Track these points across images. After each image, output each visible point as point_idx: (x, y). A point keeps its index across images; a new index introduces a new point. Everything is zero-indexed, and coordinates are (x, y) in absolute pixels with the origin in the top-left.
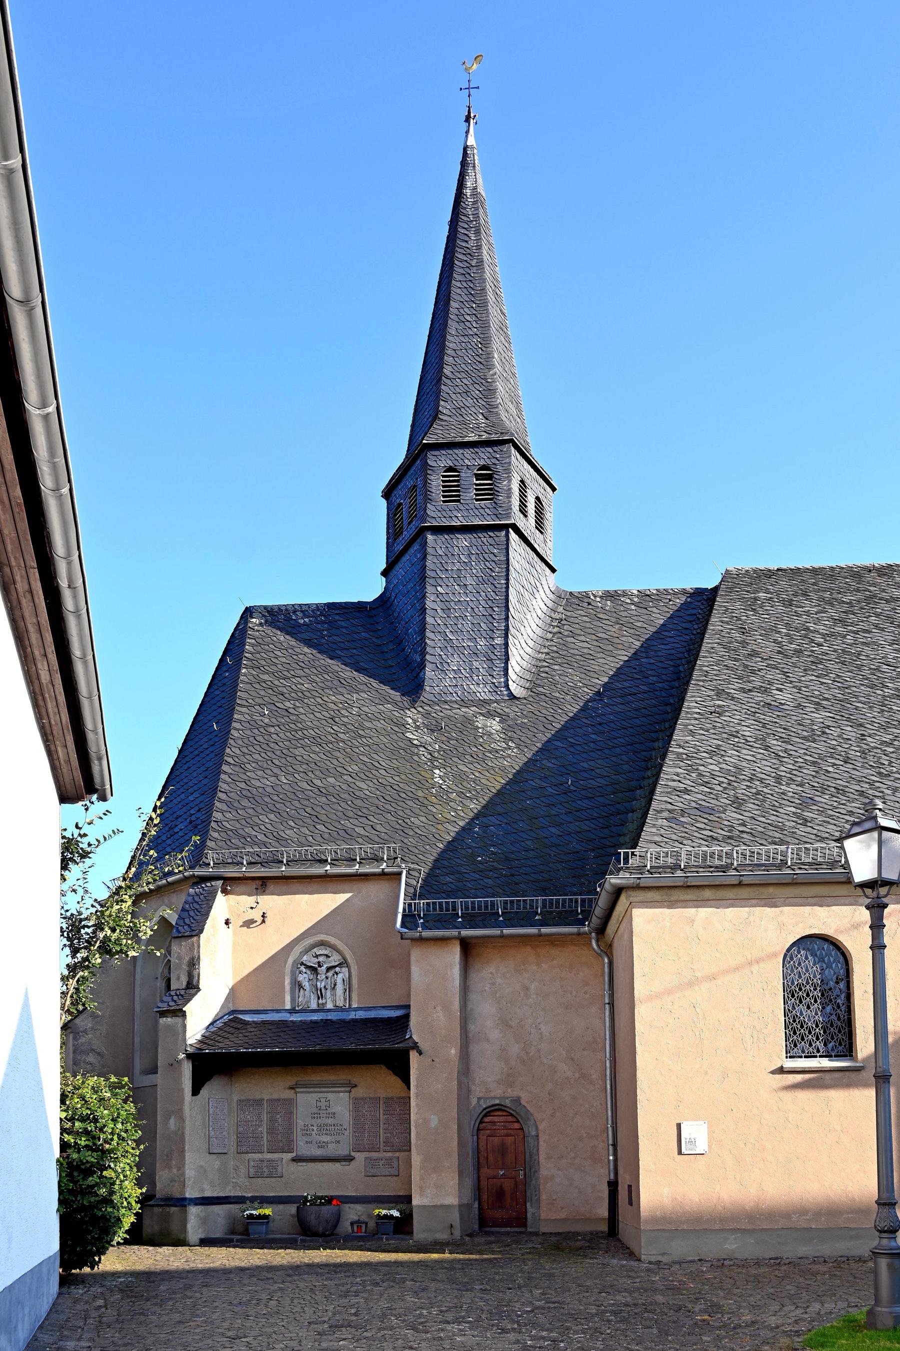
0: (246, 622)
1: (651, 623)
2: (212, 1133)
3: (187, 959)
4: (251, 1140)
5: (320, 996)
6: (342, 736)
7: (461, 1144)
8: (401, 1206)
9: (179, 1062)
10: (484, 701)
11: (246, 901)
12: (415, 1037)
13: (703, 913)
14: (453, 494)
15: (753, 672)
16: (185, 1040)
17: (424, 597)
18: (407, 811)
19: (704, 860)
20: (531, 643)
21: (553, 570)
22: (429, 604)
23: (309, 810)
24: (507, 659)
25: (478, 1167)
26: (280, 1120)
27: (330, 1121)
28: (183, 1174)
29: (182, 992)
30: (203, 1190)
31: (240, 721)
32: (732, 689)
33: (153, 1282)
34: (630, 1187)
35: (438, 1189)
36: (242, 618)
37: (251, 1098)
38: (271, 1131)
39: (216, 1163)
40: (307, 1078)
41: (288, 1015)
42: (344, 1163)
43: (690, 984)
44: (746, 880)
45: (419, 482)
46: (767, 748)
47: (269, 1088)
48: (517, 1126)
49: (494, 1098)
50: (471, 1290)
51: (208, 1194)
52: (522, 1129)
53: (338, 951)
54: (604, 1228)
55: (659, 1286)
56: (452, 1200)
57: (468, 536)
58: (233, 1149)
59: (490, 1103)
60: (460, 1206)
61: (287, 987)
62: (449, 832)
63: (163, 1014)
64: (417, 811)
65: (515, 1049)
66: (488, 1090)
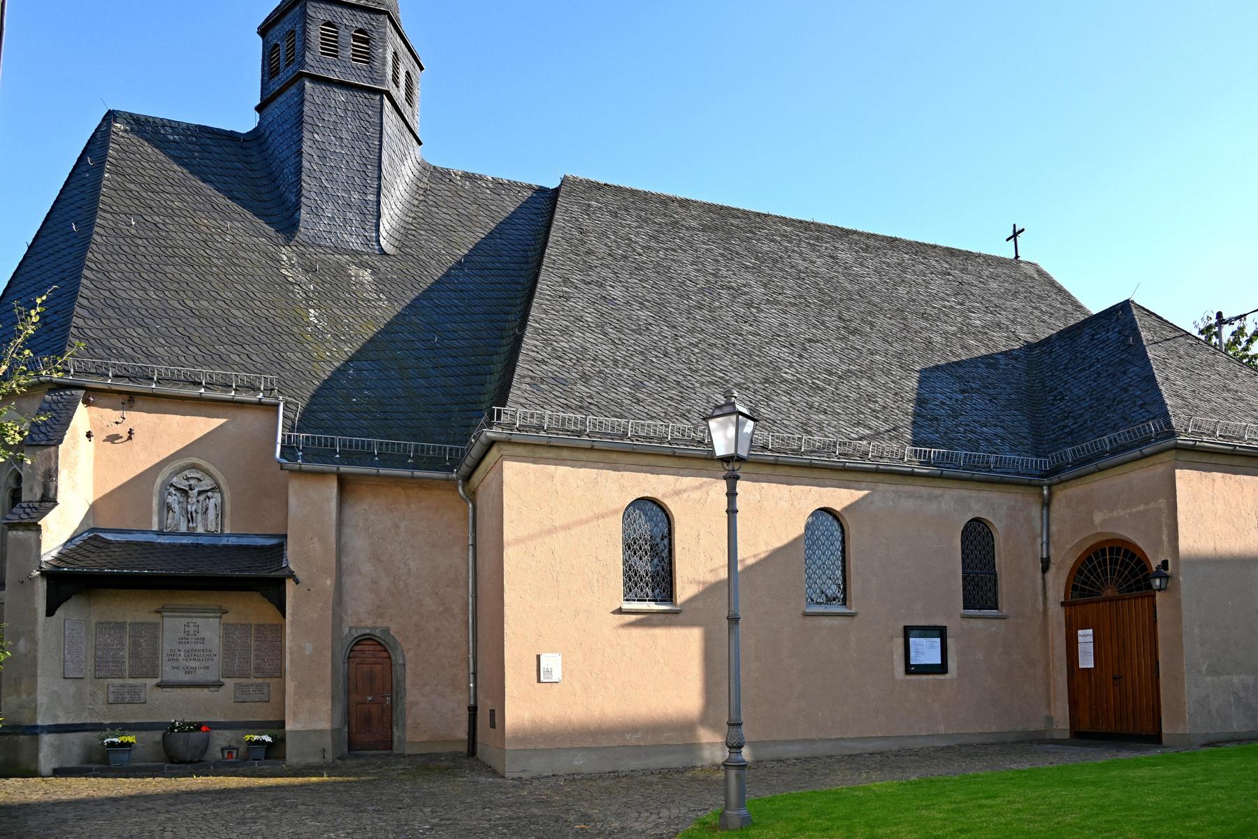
0: (109, 126)
1: (504, 208)
2: (68, 657)
3: (42, 469)
5: (191, 519)
6: (215, 261)
7: (334, 671)
8: (275, 732)
9: (32, 580)
10: (357, 252)
11: (111, 415)
12: (291, 566)
13: (562, 470)
14: (331, 47)
15: (591, 267)
16: (39, 556)
17: (301, 140)
18: (284, 346)
19: (563, 424)
20: (400, 206)
21: (420, 143)
22: (305, 148)
23: (180, 329)
24: (379, 217)
25: (348, 693)
27: (199, 646)
28: (35, 700)
29: (36, 505)
31: (103, 227)
32: (576, 278)
33: (17, 817)
34: (492, 712)
35: (311, 715)
36: (104, 119)
38: (134, 655)
39: (72, 688)
43: (550, 532)
44: (597, 445)
45: (298, 28)
46: (605, 334)
47: (133, 611)
48: (385, 654)
49: (366, 628)
50: (365, 811)
51: (62, 721)
52: (389, 657)
53: (211, 476)
54: (463, 748)
55: (530, 799)
56: (325, 725)
57: (345, 92)
58: (90, 674)
59: (360, 633)
60: (333, 731)
62: (326, 372)
63: (12, 526)
64: (293, 347)
65: (385, 582)
66: (360, 621)
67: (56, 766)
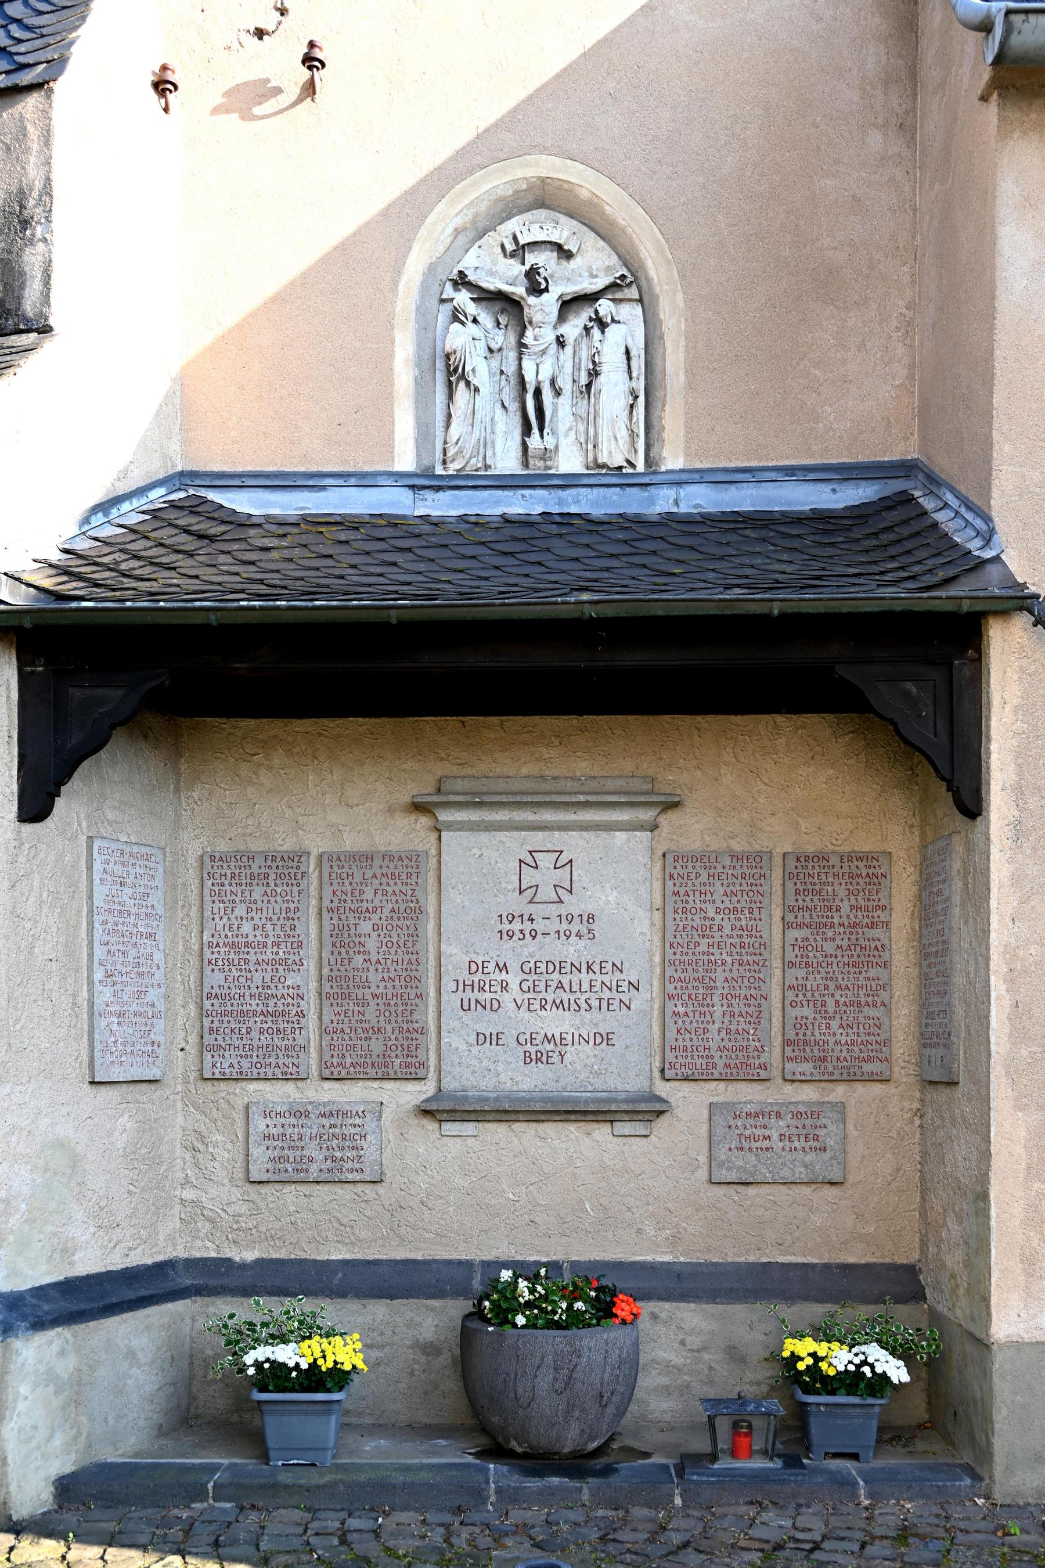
2: (104, 995)
4: (256, 1023)
5: (533, 420)
26: (372, 944)
27: (573, 950)
30: (67, 1251)
37: (256, 845)
38: (339, 987)
40: (482, 767)
41: (407, 495)
42: (626, 1128)
47: (326, 803)
51: (88, 1263)
58: (181, 1064)
61: (404, 376)
67: (65, 1465)
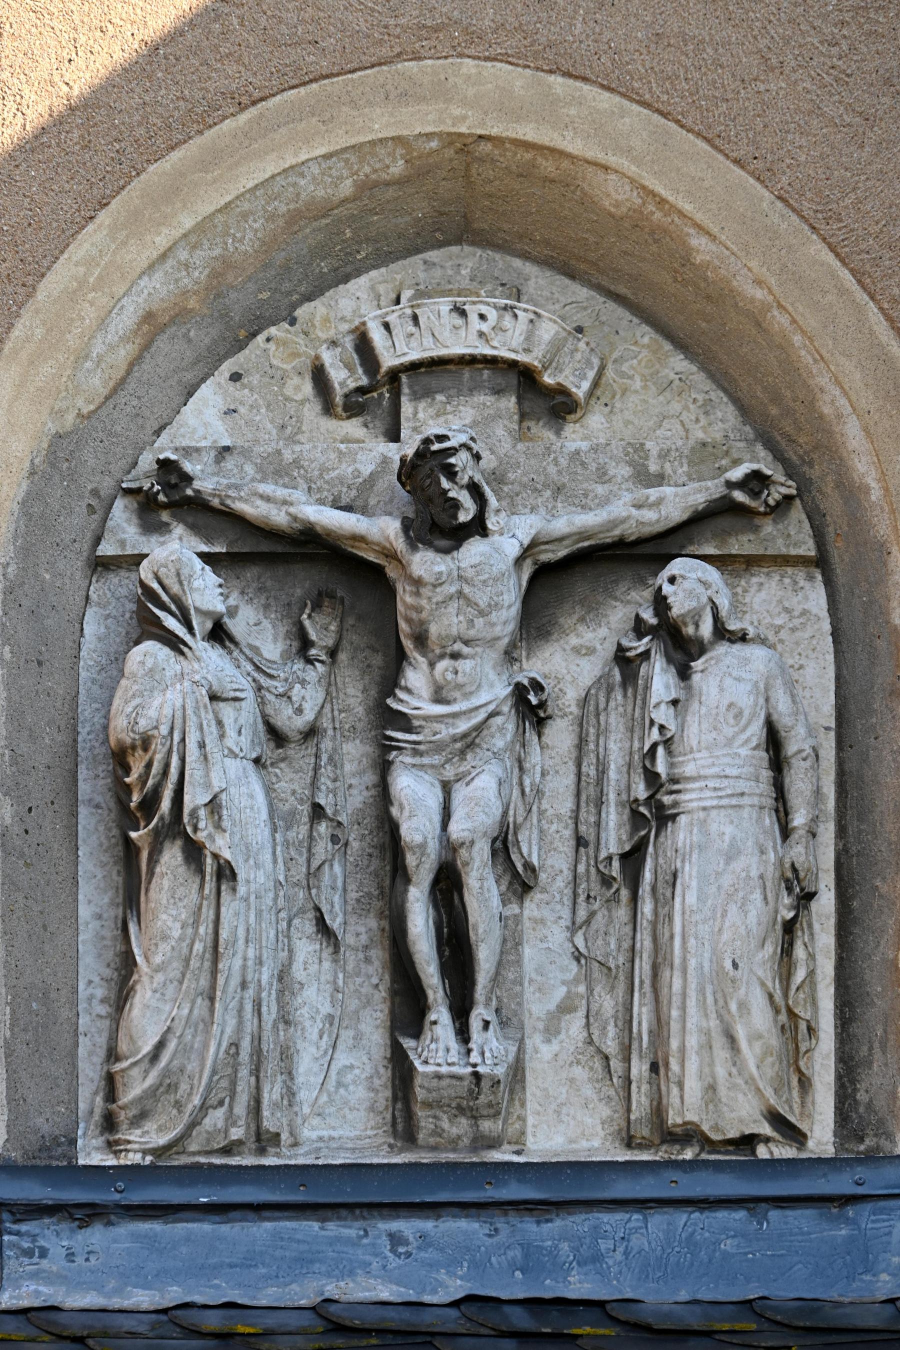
5: (430, 974)
